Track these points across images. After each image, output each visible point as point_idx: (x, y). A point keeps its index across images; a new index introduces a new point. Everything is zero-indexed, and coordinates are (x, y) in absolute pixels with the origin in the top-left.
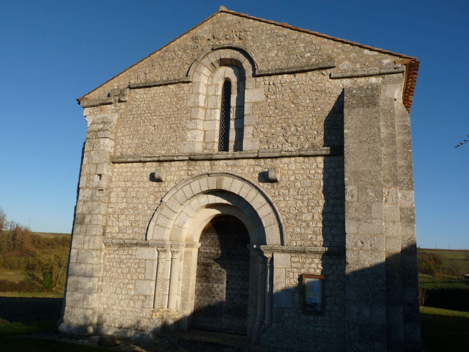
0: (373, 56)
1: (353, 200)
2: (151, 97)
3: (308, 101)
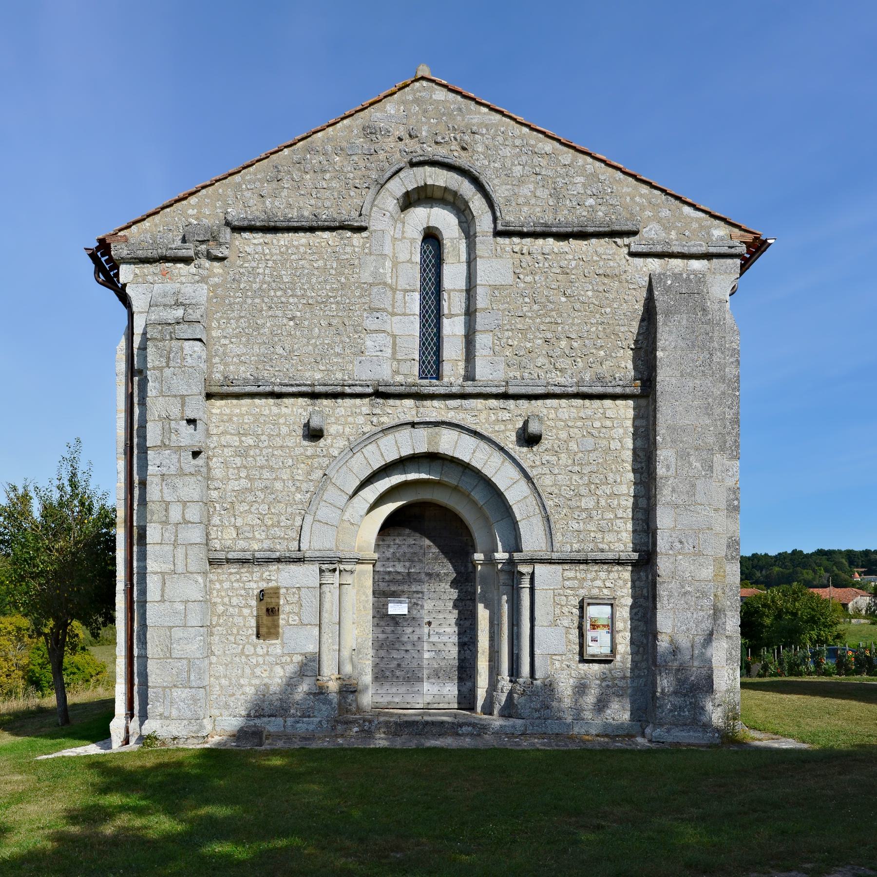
0: (697, 220)
1: (669, 473)
3: (590, 293)
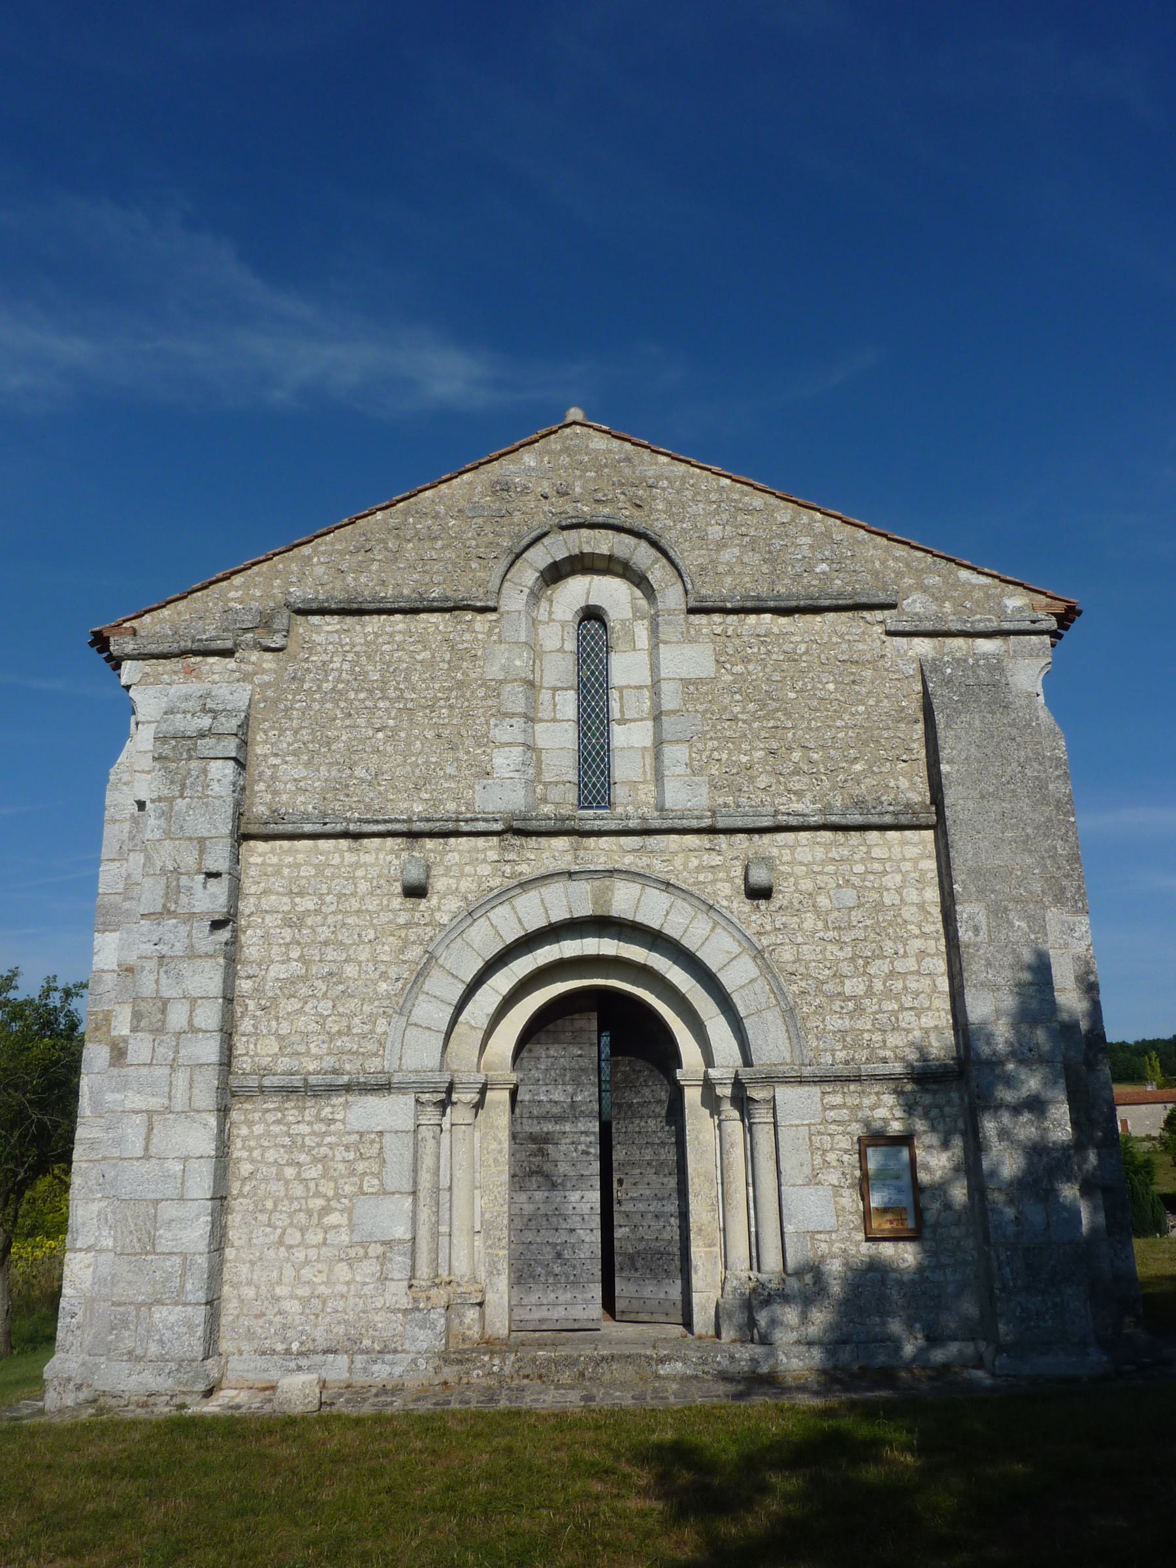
0: (981, 587)
1: (979, 939)
2: (367, 644)
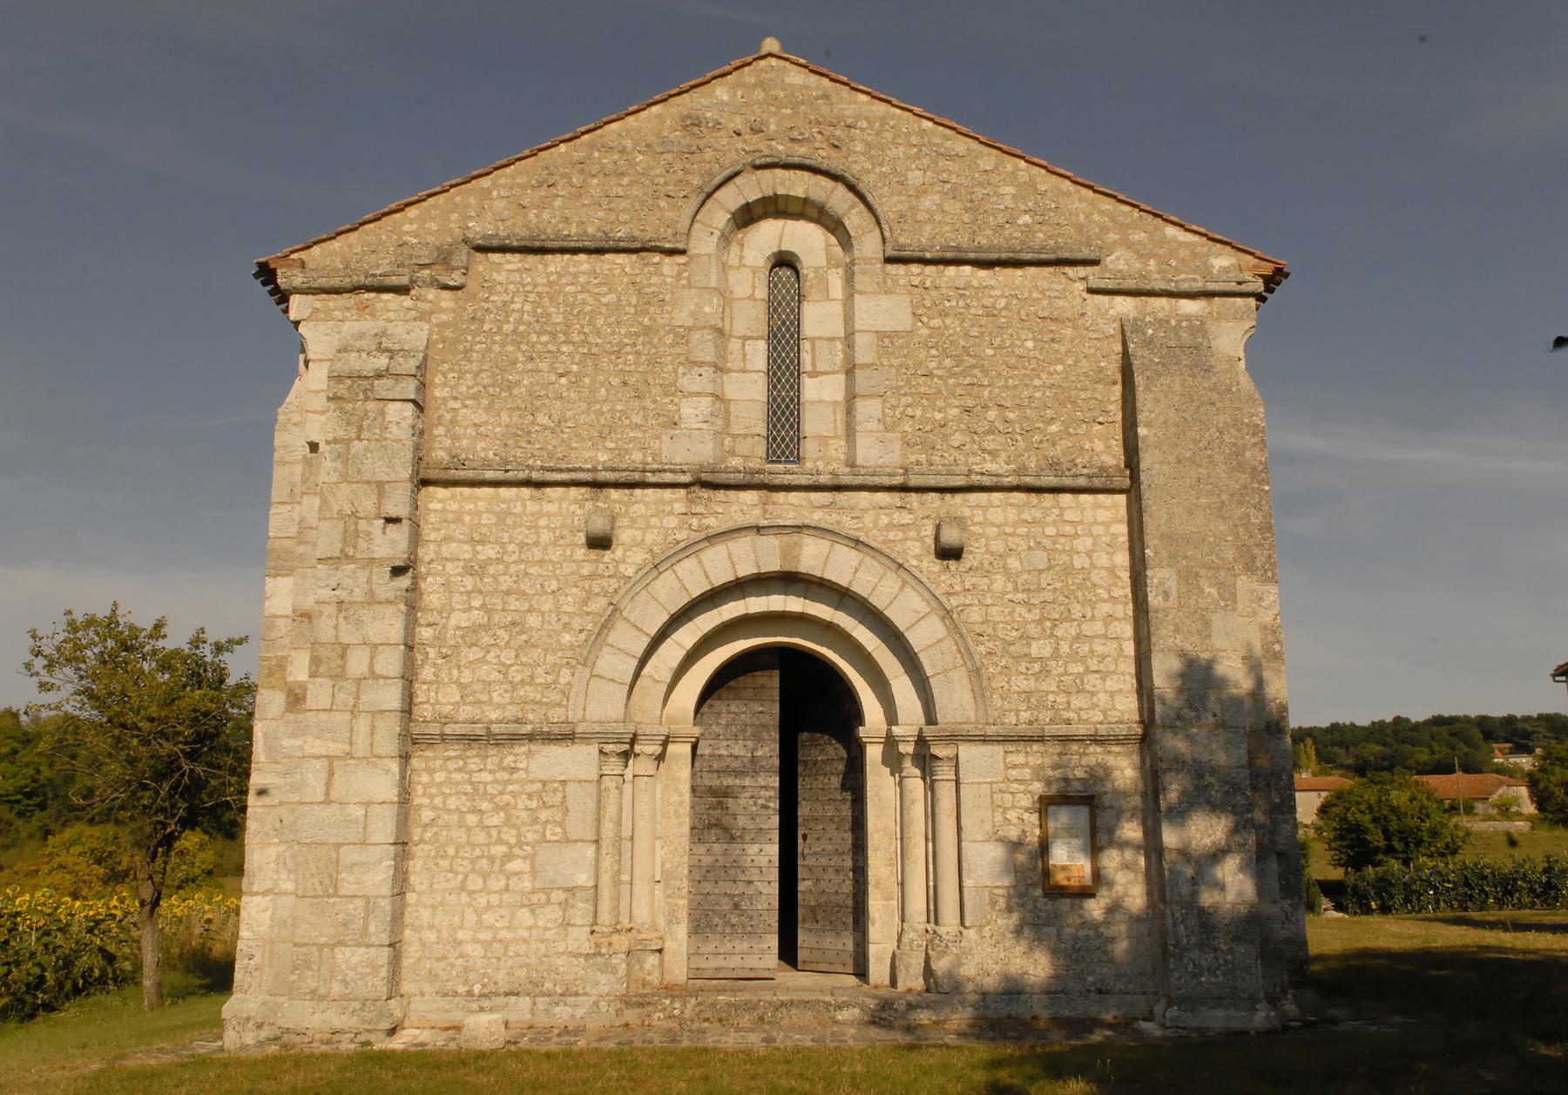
0: (1187, 245)
1: (1168, 604)
